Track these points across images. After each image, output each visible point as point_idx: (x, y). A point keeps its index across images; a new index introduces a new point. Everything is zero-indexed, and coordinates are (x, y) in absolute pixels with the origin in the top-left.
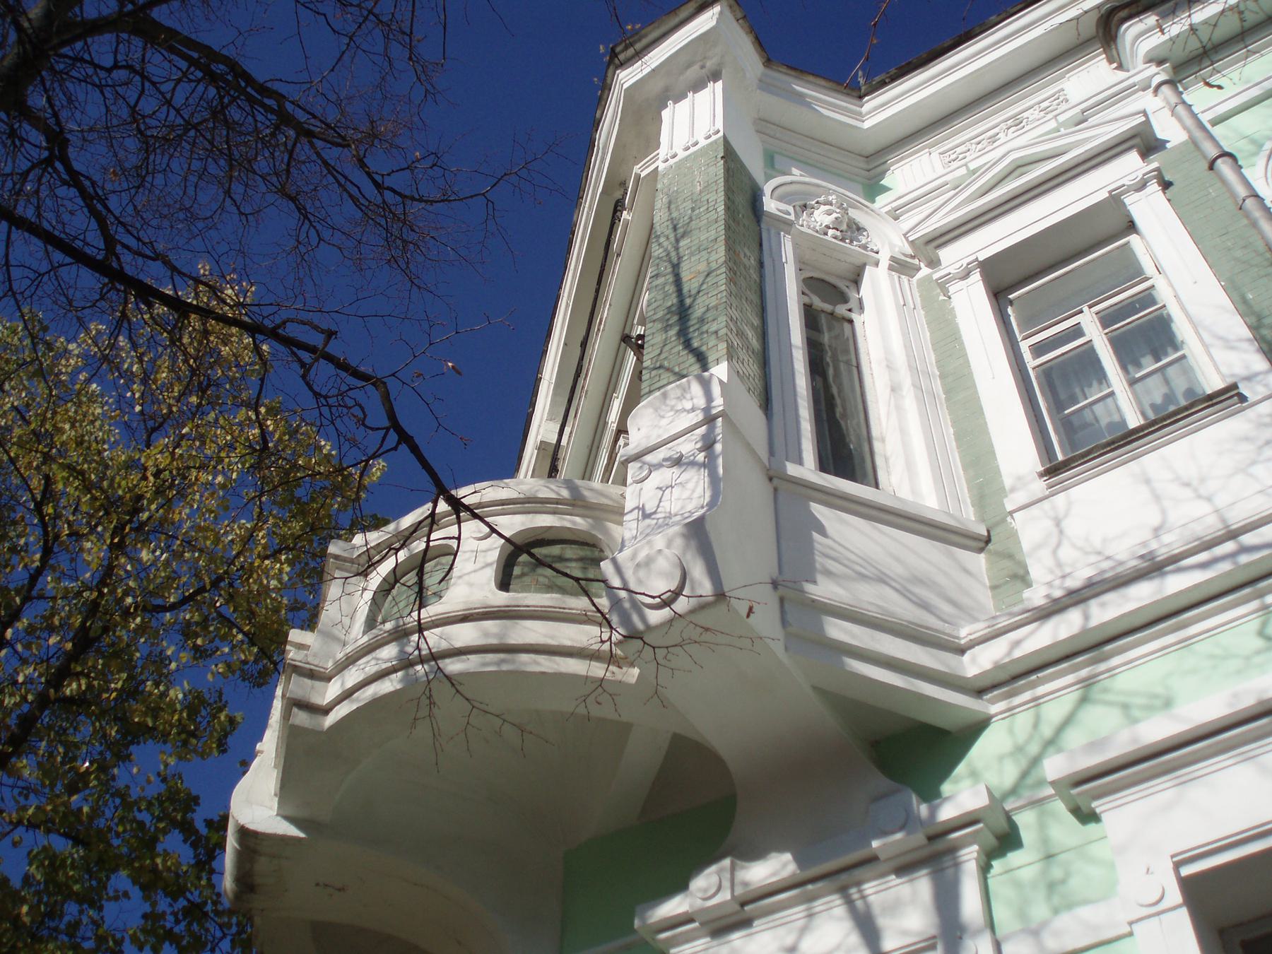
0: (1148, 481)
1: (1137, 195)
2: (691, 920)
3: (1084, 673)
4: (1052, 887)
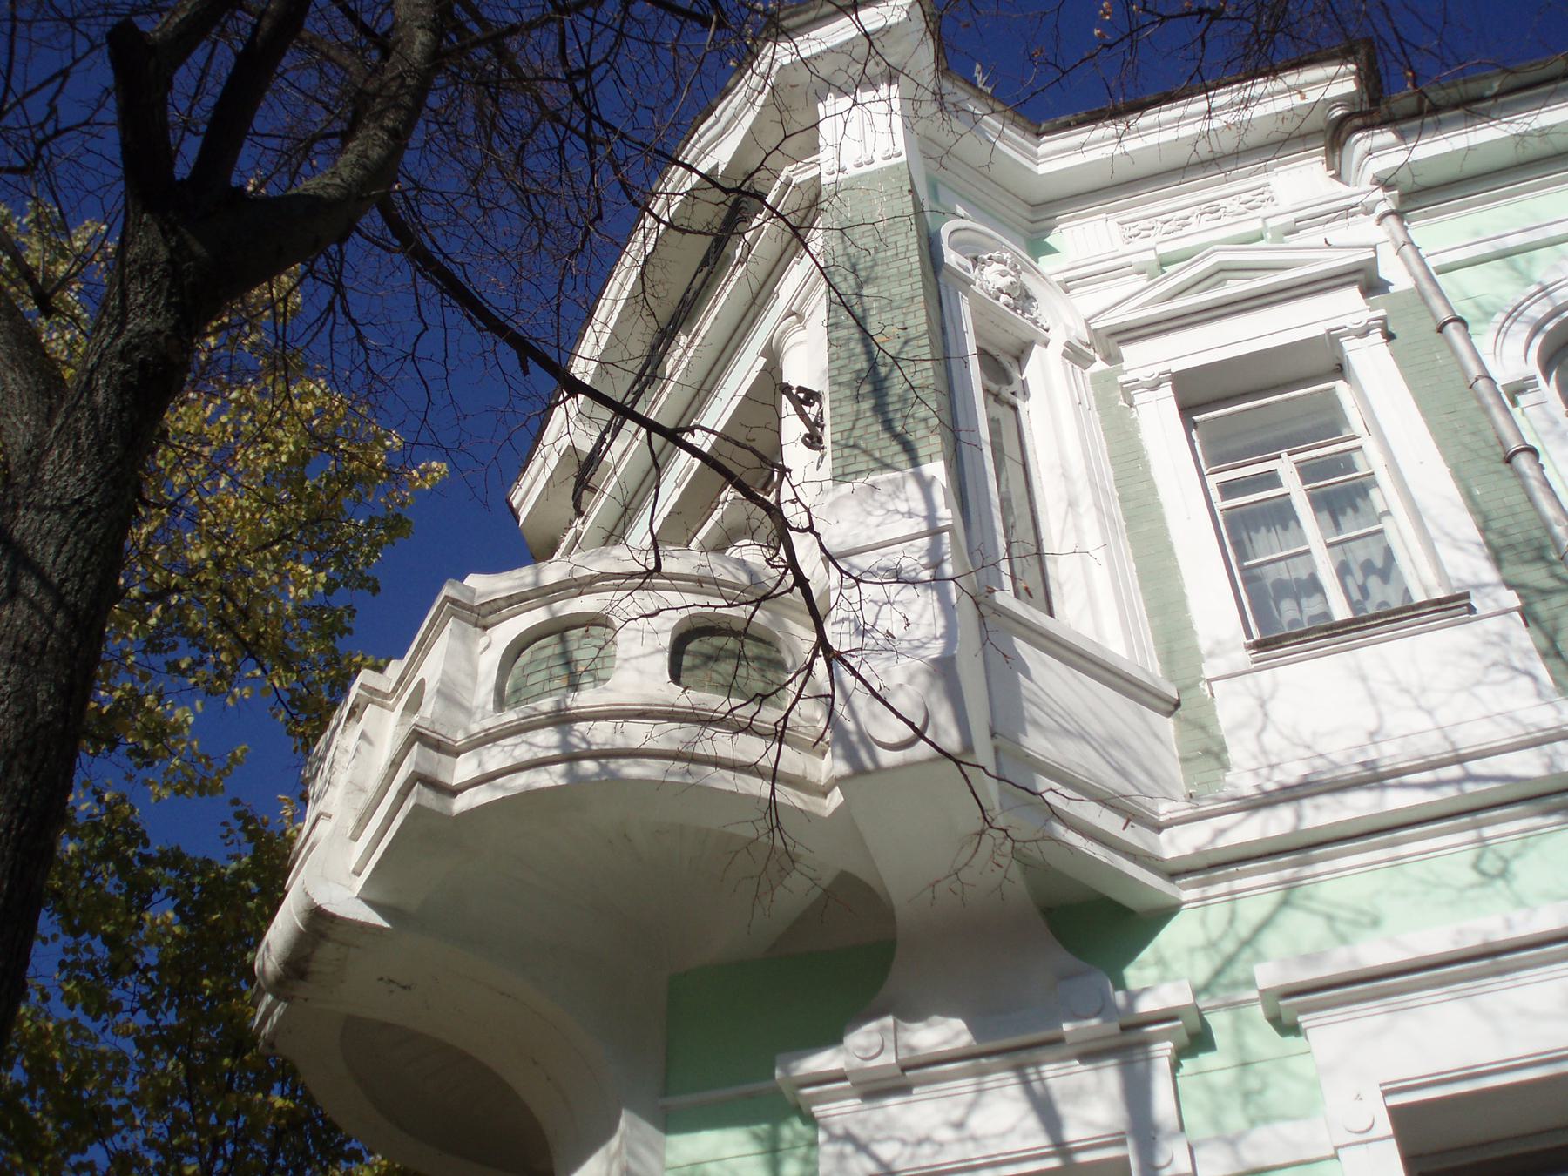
0: (1363, 679)
1: (1357, 342)
3: (1287, 873)
4: (1247, 1096)
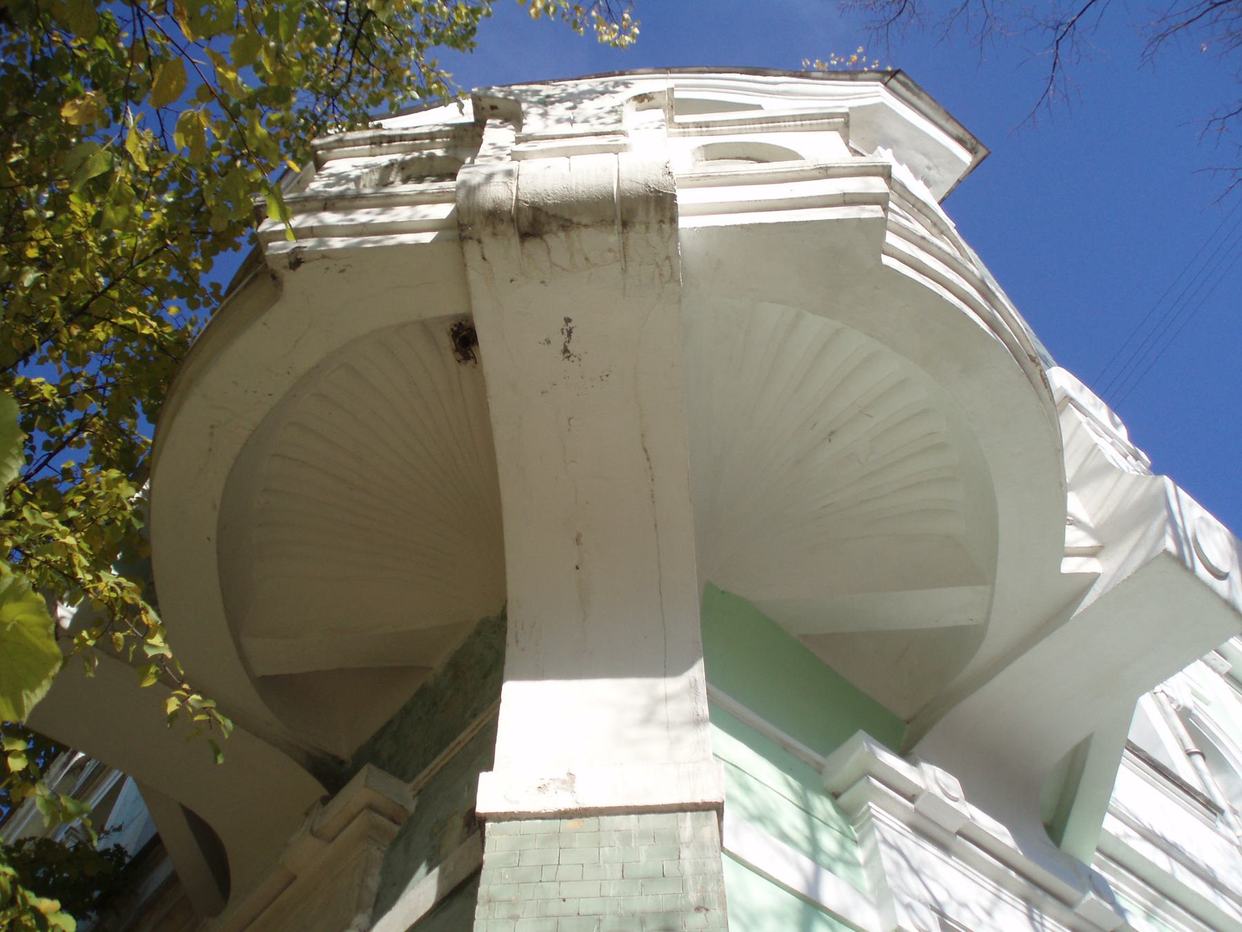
2: (912, 799)
